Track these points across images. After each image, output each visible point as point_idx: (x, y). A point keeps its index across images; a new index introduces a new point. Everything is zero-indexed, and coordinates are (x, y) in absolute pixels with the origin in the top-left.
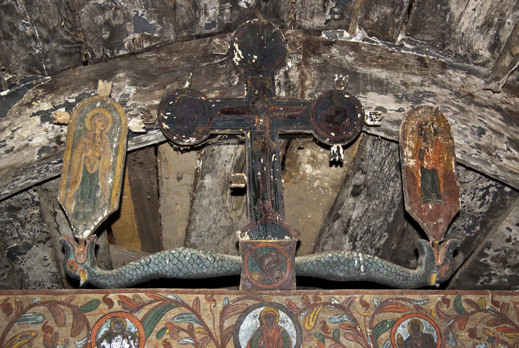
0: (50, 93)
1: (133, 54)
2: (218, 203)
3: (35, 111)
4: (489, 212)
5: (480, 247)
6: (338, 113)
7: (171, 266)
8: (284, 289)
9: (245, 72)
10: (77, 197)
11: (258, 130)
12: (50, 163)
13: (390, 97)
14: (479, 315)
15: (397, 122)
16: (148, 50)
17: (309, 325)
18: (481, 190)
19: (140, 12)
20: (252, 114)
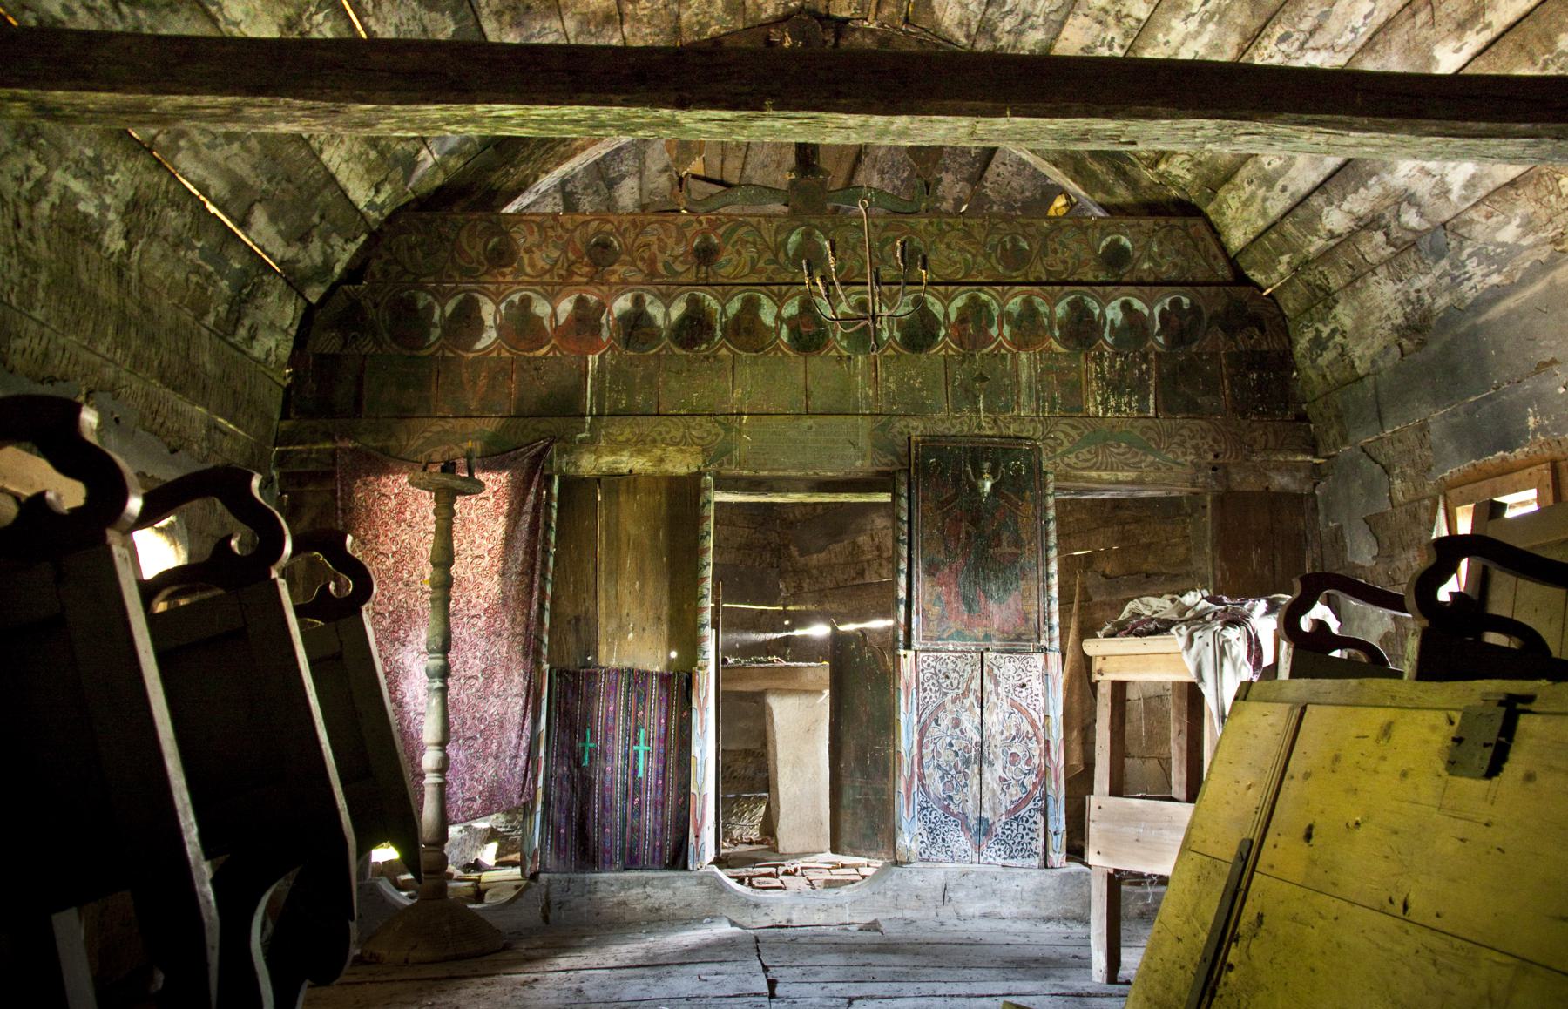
14: (953, 233)
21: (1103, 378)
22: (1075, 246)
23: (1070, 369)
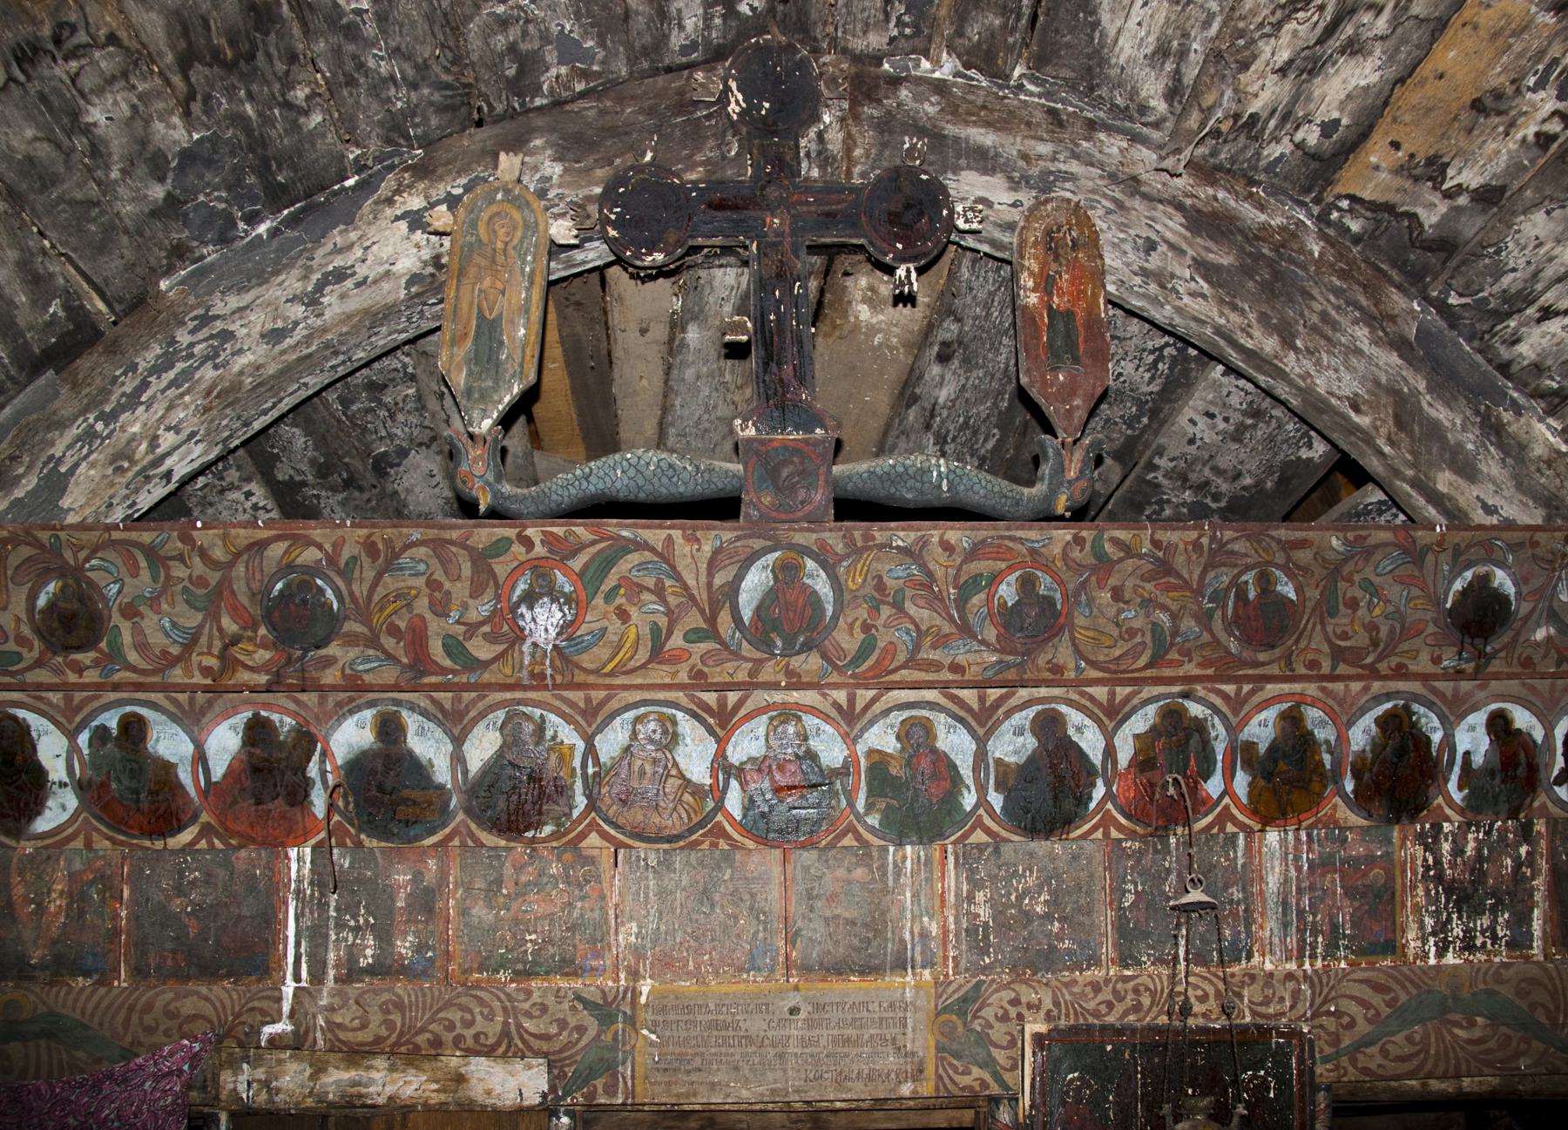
0: (422, 179)
1: (558, 103)
2: (711, 375)
3: (399, 213)
4: (1163, 391)
5: (1148, 453)
6: (908, 207)
7: (626, 481)
8: (814, 521)
9: (748, 133)
10: (468, 362)
11: (771, 238)
12: (425, 304)
13: (998, 181)
14: (1130, 564)
15: (1010, 227)
16: (583, 95)
17: (854, 582)
18: (1152, 352)
19: (568, 27)
20: (761, 208)
21: (1439, 878)
22: (1394, 592)
23: (1370, 860)
